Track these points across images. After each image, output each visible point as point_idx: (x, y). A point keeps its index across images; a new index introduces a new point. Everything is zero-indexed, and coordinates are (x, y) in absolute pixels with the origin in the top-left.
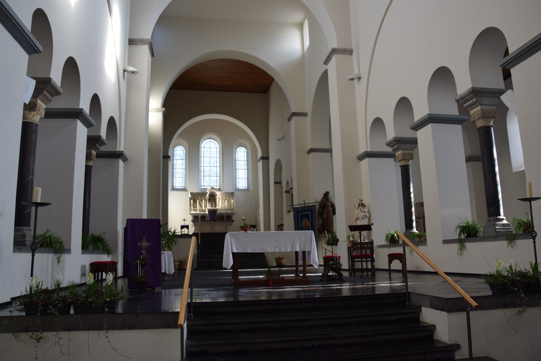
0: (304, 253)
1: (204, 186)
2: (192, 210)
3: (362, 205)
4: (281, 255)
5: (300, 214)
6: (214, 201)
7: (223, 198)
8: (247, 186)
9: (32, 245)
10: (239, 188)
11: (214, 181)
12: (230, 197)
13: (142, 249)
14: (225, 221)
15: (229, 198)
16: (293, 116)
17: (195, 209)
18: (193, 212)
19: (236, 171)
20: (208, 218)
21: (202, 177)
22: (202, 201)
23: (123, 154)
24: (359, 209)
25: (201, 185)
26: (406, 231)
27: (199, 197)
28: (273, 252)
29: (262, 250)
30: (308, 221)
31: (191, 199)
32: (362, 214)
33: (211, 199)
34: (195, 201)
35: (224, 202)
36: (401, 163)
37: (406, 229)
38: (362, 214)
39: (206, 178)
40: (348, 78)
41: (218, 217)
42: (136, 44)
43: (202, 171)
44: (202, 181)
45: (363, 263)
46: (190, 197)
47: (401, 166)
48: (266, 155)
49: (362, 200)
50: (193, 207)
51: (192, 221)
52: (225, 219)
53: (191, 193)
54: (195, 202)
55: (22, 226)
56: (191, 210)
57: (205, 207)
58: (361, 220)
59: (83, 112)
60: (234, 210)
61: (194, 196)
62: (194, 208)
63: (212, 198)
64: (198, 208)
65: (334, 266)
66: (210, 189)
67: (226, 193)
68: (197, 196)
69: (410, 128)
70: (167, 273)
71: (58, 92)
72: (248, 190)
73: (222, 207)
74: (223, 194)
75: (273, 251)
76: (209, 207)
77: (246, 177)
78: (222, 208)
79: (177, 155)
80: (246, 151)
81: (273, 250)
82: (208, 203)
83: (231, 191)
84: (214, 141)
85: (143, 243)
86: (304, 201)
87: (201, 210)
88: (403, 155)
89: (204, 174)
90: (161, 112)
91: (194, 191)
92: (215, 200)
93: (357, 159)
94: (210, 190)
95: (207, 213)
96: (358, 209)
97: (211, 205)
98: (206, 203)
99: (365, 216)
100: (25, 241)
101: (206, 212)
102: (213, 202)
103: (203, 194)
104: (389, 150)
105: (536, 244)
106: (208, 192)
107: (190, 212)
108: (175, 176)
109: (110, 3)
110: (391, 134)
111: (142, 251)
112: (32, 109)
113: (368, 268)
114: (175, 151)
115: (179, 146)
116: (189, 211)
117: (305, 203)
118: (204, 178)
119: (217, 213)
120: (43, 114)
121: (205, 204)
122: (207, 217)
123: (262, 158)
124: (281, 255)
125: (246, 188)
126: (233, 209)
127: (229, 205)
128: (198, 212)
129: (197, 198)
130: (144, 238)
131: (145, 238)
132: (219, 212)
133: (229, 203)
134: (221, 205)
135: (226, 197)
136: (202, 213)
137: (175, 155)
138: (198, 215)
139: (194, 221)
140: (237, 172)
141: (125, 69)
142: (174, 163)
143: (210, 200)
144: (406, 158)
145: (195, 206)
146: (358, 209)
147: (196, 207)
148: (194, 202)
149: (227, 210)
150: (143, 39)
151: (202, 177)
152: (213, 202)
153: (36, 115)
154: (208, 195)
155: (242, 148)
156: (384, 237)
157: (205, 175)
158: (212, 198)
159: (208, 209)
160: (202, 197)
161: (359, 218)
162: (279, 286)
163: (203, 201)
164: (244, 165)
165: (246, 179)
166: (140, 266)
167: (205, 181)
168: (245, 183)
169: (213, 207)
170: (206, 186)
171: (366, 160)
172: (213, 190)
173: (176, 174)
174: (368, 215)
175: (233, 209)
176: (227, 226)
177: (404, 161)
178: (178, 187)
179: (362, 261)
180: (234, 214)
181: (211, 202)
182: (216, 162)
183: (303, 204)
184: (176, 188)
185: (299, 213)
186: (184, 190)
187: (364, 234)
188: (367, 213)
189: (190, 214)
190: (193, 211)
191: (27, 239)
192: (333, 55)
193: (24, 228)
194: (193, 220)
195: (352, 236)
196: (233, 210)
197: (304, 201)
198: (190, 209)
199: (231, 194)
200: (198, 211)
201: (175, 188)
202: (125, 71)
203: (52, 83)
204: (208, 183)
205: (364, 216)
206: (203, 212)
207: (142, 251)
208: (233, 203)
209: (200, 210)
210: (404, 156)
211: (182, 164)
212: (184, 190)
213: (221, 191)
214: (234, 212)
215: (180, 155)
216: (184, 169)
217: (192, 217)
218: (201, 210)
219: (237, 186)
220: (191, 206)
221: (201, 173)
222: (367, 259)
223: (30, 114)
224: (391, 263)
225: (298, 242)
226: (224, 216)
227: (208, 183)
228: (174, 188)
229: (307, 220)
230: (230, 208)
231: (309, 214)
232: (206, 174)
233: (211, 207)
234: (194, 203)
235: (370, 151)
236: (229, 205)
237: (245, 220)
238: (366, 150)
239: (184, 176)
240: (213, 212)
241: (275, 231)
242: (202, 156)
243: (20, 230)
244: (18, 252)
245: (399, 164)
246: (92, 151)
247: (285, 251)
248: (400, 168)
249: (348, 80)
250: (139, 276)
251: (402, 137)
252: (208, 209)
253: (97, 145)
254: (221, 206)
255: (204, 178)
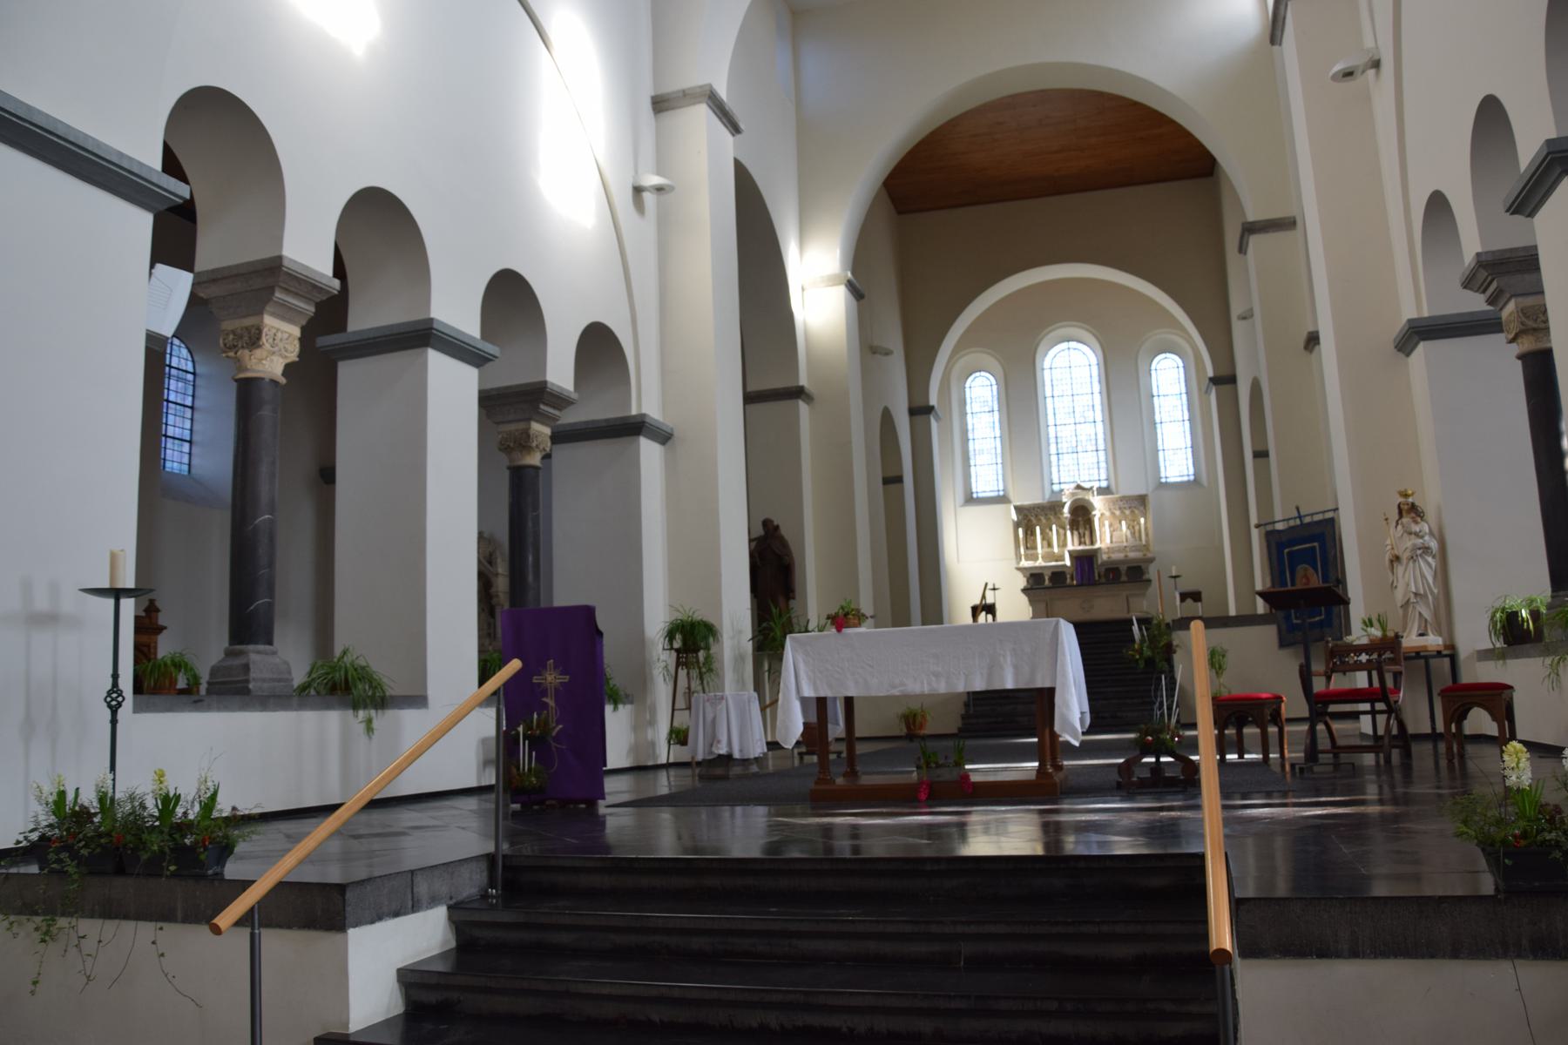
0: (849, 701)
1: (1060, 483)
2: (1023, 558)
3: (1410, 510)
4: (1225, 687)
5: (1286, 551)
6: (1088, 526)
7: (1113, 514)
8: (1191, 471)
9: (109, 699)
10: (1169, 480)
11: (1091, 466)
12: (1136, 512)
13: (544, 693)
14: (1124, 582)
15: (1132, 512)
16: (1246, 234)
17: (1031, 555)
18: (1025, 563)
19: (1155, 428)
20: (1072, 579)
21: (1054, 458)
22: (1051, 530)
23: (644, 422)
24: (1399, 527)
25: (1051, 480)
26: (1552, 597)
27: (1042, 518)
28: (926, 692)
29: (894, 687)
30: (1315, 575)
31: (1017, 525)
32: (1410, 542)
33: (1078, 522)
34: (1032, 531)
35: (1118, 525)
36: (1521, 345)
37: (1554, 591)
38: (1410, 542)
39: (1067, 460)
40: (1331, 74)
41: (1102, 573)
42: (673, 108)
43: (1052, 440)
44: (1054, 470)
45: (1378, 716)
46: (1016, 519)
47: (1520, 357)
48: (1224, 372)
49: (1410, 492)
50: (1027, 548)
51: (1025, 590)
52: (1124, 578)
53: (1016, 508)
54: (1029, 532)
55: (248, 644)
56: (1018, 557)
57: (1062, 548)
58: (1407, 563)
59: (435, 326)
60: (1151, 548)
61: (1027, 516)
62: (1030, 552)
63: (1081, 516)
64: (1039, 550)
65: (1150, 738)
66: (1071, 491)
67: (1123, 499)
68: (1036, 516)
69: (1507, 211)
70: (737, 755)
71: (321, 288)
72: (1196, 482)
73: (1111, 542)
74: (1114, 502)
75: (926, 690)
76: (1073, 544)
77: (1189, 444)
78: (1114, 545)
79: (973, 400)
80: (1181, 364)
81: (926, 685)
82: (1069, 533)
83: (1139, 490)
84: (1080, 346)
85: (547, 676)
86: (1298, 509)
87: (1049, 556)
88: (1524, 314)
89: (1059, 446)
90: (840, 284)
91: (1027, 502)
92: (1089, 523)
93: (1395, 350)
94: (1073, 494)
95: (1068, 562)
96: (1397, 524)
97: (1080, 537)
98: (1065, 535)
99: (1419, 549)
100: (247, 681)
101: (1064, 560)
102: (1085, 529)
103: (1054, 507)
104: (1476, 303)
105: (119, 726)
106: (1067, 501)
107: (1018, 563)
108: (972, 462)
109: (534, 13)
110: (1471, 244)
111: (545, 699)
112: (254, 344)
113: (1438, 731)
114: (967, 390)
115: (978, 374)
116: (1014, 561)
117: (1302, 514)
118: (1059, 460)
119: (1100, 562)
120: (292, 352)
121: (1062, 537)
122: (1068, 576)
123: (1215, 381)
124: (1225, 687)
125: (1192, 478)
126: (1146, 547)
127: (1135, 532)
128: (1040, 563)
129: (1034, 521)
130: (548, 663)
131: (552, 661)
132: (1105, 557)
133: (1133, 527)
134: (1109, 535)
135: (1122, 512)
136: (1053, 563)
137: (968, 401)
138: (1139, 564)
139: (1031, 589)
140: (1159, 431)
141: (637, 185)
142: (966, 424)
143: (1074, 525)
144: (1535, 326)
145: (1030, 546)
146: (1397, 524)
147: (1035, 548)
148: (1029, 532)
149: (1128, 549)
150: (689, 89)
151: (1052, 456)
152: (1085, 529)
153: (267, 357)
154: (1066, 510)
155: (1168, 355)
156: (1485, 622)
157: (1060, 451)
158: (1080, 519)
159: (1069, 552)
160: (1050, 519)
161: (1400, 554)
162: (930, 807)
163: (1054, 527)
164: (1180, 407)
165: (1189, 450)
166: (527, 742)
167: (1061, 468)
168: (1185, 462)
169: (1085, 544)
170: (1065, 483)
171: (1422, 348)
172: (1081, 494)
173: (977, 456)
174: (1434, 544)
175: (1146, 547)
176: (1131, 600)
177: (1531, 338)
178: (984, 492)
179: (1373, 713)
180: (1151, 560)
181: (1077, 529)
182: (1091, 408)
183: (1295, 518)
184: (980, 495)
185: (1285, 548)
186: (1002, 499)
187: (1420, 614)
188: (1427, 538)
189: (1019, 569)
190: (1027, 559)
191: (252, 675)
192: (1286, 5)
193: (251, 647)
194: (1029, 586)
195: (1379, 621)
196: (1148, 549)
197: (1298, 509)
198: (1016, 555)
199: (1136, 500)
200: (1040, 560)
201: (975, 496)
202: (638, 190)
203: (289, 269)
204: (1072, 473)
205: (1415, 548)
206: (1057, 561)
207: (545, 699)
208: (1146, 529)
209: (1046, 557)
210: (1528, 317)
211: (992, 425)
212: (1002, 499)
213: (1112, 494)
214: (1149, 555)
215: (982, 400)
216: (998, 440)
217: (1025, 579)
218: (1049, 556)
219: (1163, 475)
220: (1019, 547)
221: (1049, 444)
222: (1373, 706)
223: (252, 357)
224: (1465, 718)
225: (1009, 659)
226: (1121, 569)
227: (1072, 473)
228: (972, 497)
229: (1311, 571)
230: (1138, 543)
231: (1314, 548)
232: (1064, 447)
233: (1080, 544)
234: (1028, 537)
235: (1429, 318)
236: (1133, 534)
237: (1177, 579)
238: (1415, 316)
239: (999, 461)
240: (1085, 561)
241: (876, 627)
242: (1048, 393)
243: (241, 653)
244: (190, 711)
245: (1515, 349)
246: (530, 425)
247: (1016, 680)
248: (1519, 363)
249: (1334, 78)
250: (524, 769)
251: (1511, 250)
252: (1069, 552)
253: (542, 407)
254: (1108, 541)
255: (1059, 460)
